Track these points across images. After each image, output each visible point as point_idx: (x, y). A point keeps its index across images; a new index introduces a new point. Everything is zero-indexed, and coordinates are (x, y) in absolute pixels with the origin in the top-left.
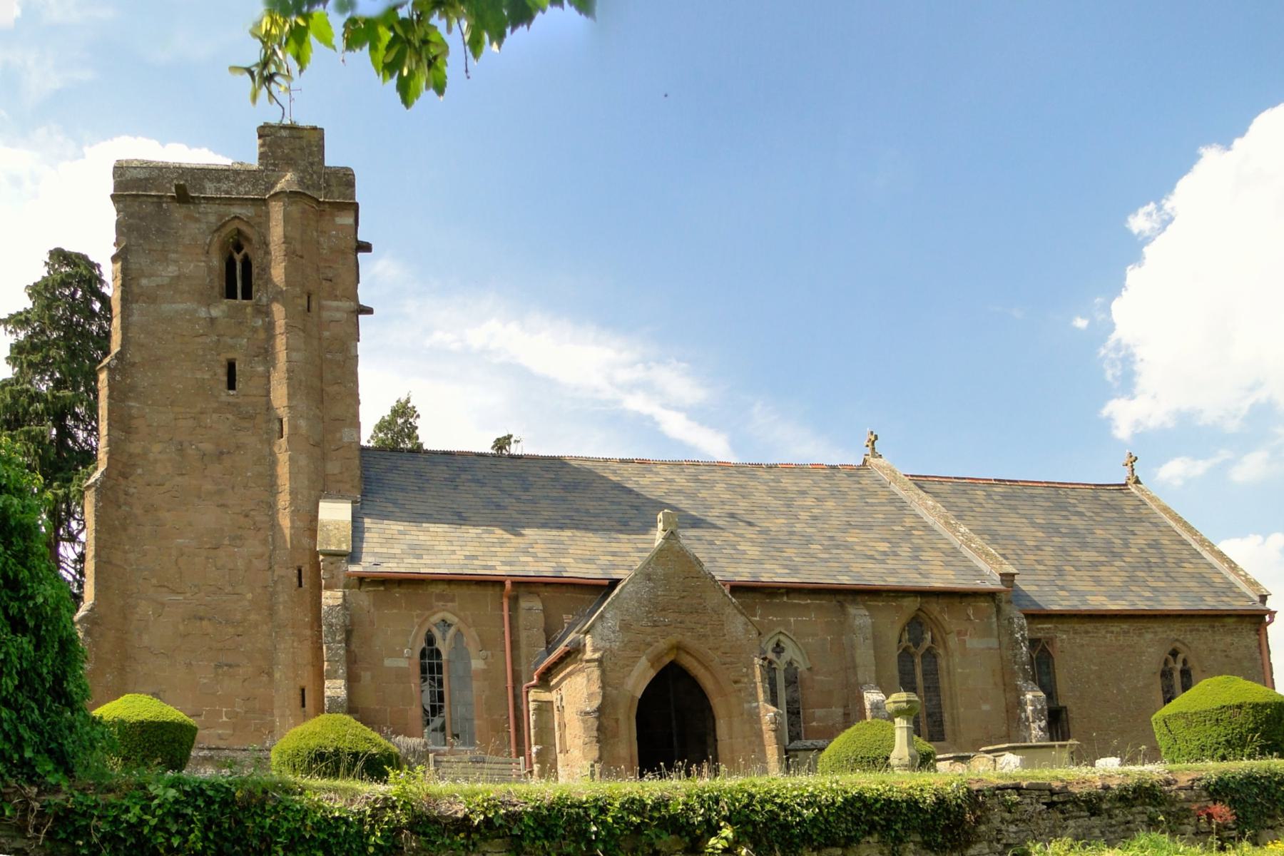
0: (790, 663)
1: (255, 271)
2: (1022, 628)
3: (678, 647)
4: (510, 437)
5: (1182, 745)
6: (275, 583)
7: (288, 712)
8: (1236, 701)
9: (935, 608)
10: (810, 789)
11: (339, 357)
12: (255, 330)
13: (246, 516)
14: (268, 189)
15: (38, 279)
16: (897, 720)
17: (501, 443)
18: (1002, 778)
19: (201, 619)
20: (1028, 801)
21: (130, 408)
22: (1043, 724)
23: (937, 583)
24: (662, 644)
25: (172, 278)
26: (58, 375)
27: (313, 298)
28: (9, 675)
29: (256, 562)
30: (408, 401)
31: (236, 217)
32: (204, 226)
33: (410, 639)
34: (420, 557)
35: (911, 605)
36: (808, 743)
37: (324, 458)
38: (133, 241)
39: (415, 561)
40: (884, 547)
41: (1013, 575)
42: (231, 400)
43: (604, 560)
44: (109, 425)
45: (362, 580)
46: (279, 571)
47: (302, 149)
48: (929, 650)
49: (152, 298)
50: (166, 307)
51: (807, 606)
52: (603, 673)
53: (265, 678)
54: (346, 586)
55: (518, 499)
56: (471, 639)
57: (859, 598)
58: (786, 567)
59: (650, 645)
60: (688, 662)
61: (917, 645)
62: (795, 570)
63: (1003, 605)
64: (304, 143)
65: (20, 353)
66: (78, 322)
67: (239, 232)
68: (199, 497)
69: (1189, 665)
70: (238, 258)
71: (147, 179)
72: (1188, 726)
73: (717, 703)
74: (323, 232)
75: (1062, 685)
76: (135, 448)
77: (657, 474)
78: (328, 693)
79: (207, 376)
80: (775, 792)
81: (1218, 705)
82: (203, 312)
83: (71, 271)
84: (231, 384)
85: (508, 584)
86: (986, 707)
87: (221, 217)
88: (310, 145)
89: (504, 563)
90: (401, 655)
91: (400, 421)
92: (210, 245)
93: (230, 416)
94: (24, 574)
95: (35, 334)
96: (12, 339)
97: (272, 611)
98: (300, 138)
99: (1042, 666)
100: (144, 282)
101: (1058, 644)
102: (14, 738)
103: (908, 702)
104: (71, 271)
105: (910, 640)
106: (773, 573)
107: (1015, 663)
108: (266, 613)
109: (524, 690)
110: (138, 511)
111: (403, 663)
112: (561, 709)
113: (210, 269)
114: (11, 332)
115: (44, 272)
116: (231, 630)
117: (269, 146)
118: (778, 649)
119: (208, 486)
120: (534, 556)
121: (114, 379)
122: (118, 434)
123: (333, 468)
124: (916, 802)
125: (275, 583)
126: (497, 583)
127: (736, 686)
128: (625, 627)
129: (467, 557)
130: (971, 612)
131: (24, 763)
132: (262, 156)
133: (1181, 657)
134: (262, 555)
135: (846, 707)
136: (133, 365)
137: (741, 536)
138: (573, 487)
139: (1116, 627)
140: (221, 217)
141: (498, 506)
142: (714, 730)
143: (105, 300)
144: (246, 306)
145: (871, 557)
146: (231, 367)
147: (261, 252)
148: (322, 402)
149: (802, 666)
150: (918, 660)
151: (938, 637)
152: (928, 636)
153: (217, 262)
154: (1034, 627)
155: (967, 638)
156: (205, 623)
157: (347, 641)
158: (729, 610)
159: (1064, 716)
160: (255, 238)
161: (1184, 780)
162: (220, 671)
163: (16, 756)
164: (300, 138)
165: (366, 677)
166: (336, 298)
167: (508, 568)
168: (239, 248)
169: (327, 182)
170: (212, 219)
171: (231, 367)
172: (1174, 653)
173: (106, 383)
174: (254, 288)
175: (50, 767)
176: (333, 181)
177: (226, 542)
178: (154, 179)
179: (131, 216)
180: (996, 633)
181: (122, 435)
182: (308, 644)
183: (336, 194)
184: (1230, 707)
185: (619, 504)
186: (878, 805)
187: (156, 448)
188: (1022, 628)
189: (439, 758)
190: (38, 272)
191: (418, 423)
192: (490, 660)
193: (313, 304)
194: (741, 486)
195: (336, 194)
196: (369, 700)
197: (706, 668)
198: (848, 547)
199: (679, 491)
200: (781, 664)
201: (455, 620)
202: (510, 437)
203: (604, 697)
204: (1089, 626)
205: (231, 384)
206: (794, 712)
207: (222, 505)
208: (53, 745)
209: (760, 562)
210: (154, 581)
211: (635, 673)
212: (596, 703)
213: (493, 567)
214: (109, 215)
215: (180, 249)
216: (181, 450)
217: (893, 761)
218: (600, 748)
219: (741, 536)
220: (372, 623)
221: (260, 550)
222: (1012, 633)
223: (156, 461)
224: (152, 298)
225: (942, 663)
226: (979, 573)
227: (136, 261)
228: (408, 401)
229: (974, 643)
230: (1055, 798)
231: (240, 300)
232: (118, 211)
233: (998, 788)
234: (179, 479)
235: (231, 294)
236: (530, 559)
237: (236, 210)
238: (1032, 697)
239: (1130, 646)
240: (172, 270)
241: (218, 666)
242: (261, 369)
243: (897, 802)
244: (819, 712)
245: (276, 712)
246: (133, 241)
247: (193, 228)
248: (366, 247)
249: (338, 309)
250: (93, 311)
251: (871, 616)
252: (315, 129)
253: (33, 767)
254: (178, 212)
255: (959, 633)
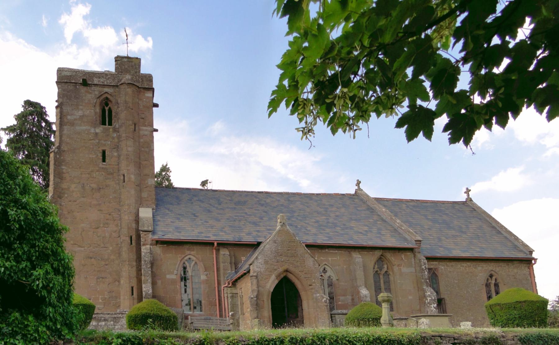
0: (329, 277)
1: (113, 114)
2: (425, 264)
3: (287, 271)
4: (207, 180)
5: (499, 318)
6: (121, 243)
7: (126, 298)
8: (523, 300)
9: (388, 255)
10: (359, 334)
11: (147, 150)
12: (113, 138)
13: (110, 215)
14: (118, 82)
15: (19, 112)
16: (383, 304)
17: (204, 183)
18: (433, 332)
19: (91, 258)
20: (445, 342)
21: (63, 169)
22: (435, 305)
23: (389, 244)
24: (281, 270)
25: (80, 116)
26: (26, 153)
27: (137, 126)
28: (54, 293)
29: (114, 234)
30: (167, 165)
31: (106, 93)
32: (93, 96)
33: (177, 266)
34: (180, 232)
35: (378, 253)
36: (339, 311)
37: (141, 191)
38: (65, 100)
39: (178, 234)
40: (366, 228)
41: (420, 241)
42: (104, 166)
43: (255, 234)
44: (54, 176)
45: (158, 242)
46: (123, 238)
47: (132, 66)
48: (386, 272)
49: (72, 124)
50: (78, 128)
51: (336, 253)
52: (258, 281)
53: (117, 283)
54: (151, 245)
55: (217, 208)
56: (201, 266)
57: (357, 250)
58: (327, 237)
59: (276, 270)
60: (291, 276)
61: (381, 270)
62: (330, 238)
63: (417, 254)
64: (133, 64)
65: (11, 143)
66: (36, 131)
67: (107, 98)
68: (91, 207)
69: (498, 281)
70: (107, 108)
71: (71, 76)
72: (502, 309)
73: (303, 294)
74: (141, 99)
75: (442, 289)
76: (64, 185)
77: (273, 198)
78: (144, 289)
79: (94, 156)
80: (346, 336)
81: (515, 301)
82: (92, 130)
83: (33, 110)
84: (104, 160)
85: (216, 244)
86: (410, 297)
87: (100, 92)
88: (135, 65)
89: (214, 235)
90: (172, 273)
91: (164, 173)
92: (96, 103)
93: (103, 173)
94: (60, 249)
95: (17, 135)
96: (7, 137)
97: (120, 254)
98: (132, 62)
99: (434, 279)
100: (69, 117)
101: (440, 271)
102: (54, 320)
103: (388, 297)
104: (33, 110)
105: (378, 268)
106: (321, 240)
107: (423, 279)
108: (118, 255)
109: (222, 288)
110: (65, 212)
111: (174, 277)
112: (242, 297)
113: (96, 113)
114: (7, 134)
115: (22, 109)
116: (103, 263)
117: (120, 65)
118: (325, 271)
119: (95, 202)
120: (225, 232)
121: (56, 157)
122: (58, 180)
123: (145, 195)
124: (401, 341)
125: (121, 243)
126: (210, 244)
127: (311, 287)
128: (266, 262)
129: (199, 233)
130: (403, 257)
131: (57, 330)
132: (116, 69)
133: (494, 278)
134: (116, 231)
135: (352, 296)
136: (64, 151)
137: (308, 224)
138: (239, 203)
139: (465, 264)
140: (100, 92)
141: (209, 211)
142: (302, 305)
143: (49, 124)
144: (110, 128)
145: (361, 233)
146: (104, 153)
147: (116, 107)
148: (140, 168)
149: (334, 278)
150: (381, 277)
151: (390, 267)
152: (385, 266)
153: (98, 110)
154: (430, 263)
155: (402, 268)
156: (93, 260)
157: (152, 267)
158: (307, 255)
159: (443, 302)
160: (113, 101)
161: (510, 336)
162: (99, 280)
163: (54, 328)
164: (132, 62)
165: (159, 282)
166: (145, 126)
167: (215, 237)
168: (107, 105)
169: (142, 79)
170: (97, 93)
171: (104, 153)
172: (491, 276)
173: (53, 158)
174: (113, 121)
175: (66, 332)
176: (144, 79)
177: (102, 225)
178: (74, 76)
179: (64, 90)
180: (414, 266)
181: (59, 180)
182: (135, 268)
183: (146, 84)
184: (520, 302)
185: (258, 210)
186: (386, 342)
187: (73, 186)
188: (425, 264)
189: (193, 318)
190: (20, 110)
191: (171, 174)
192: (208, 275)
193: (137, 128)
194: (307, 203)
195: (146, 84)
196: (161, 292)
197: (298, 279)
198: (351, 228)
199: (282, 205)
200: (326, 276)
201: (194, 258)
202: (207, 180)
203: (258, 291)
204: (453, 263)
205: (104, 160)
206: (332, 298)
207: (101, 210)
208: (68, 322)
209: (316, 234)
210: (72, 242)
211: (270, 281)
212: (255, 294)
213: (209, 237)
214: (55, 90)
215: (84, 104)
216: (83, 187)
217: (382, 320)
218: (258, 313)
219: (308, 224)
220: (161, 260)
221: (115, 229)
222: (421, 266)
223: (73, 191)
224: (72, 124)
225: (391, 278)
226: (406, 240)
227: (66, 109)
228: (167, 165)
229: (405, 270)
230: (456, 341)
231: (107, 126)
232: (59, 88)
233: (433, 336)
234: (83, 199)
235: (104, 123)
236: (223, 233)
237: (106, 90)
238: (430, 294)
239: (471, 273)
240: (80, 113)
241: (98, 278)
242: (116, 154)
243: (393, 341)
244: (342, 298)
245: (122, 297)
246: (65, 100)
247: (89, 96)
248: (156, 105)
249: (146, 130)
250: (42, 126)
251: (362, 258)
252: (137, 58)
253: (61, 332)
254: (83, 89)
255: (398, 266)
